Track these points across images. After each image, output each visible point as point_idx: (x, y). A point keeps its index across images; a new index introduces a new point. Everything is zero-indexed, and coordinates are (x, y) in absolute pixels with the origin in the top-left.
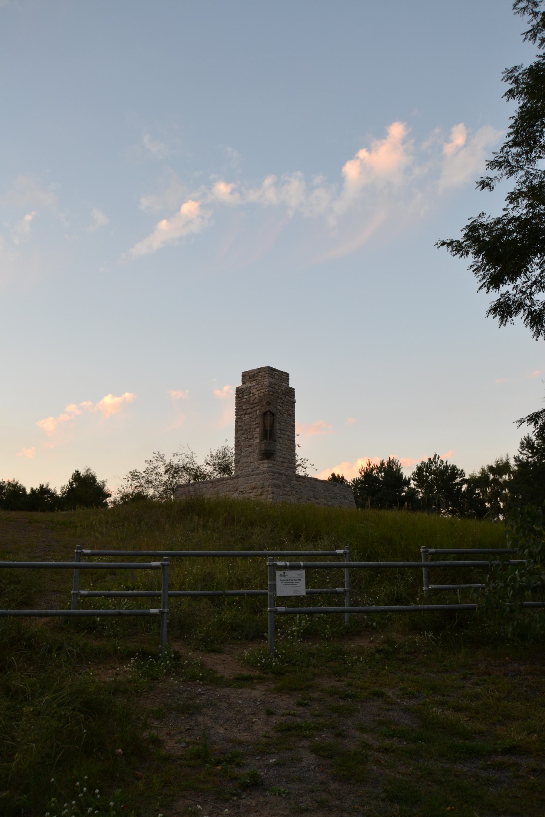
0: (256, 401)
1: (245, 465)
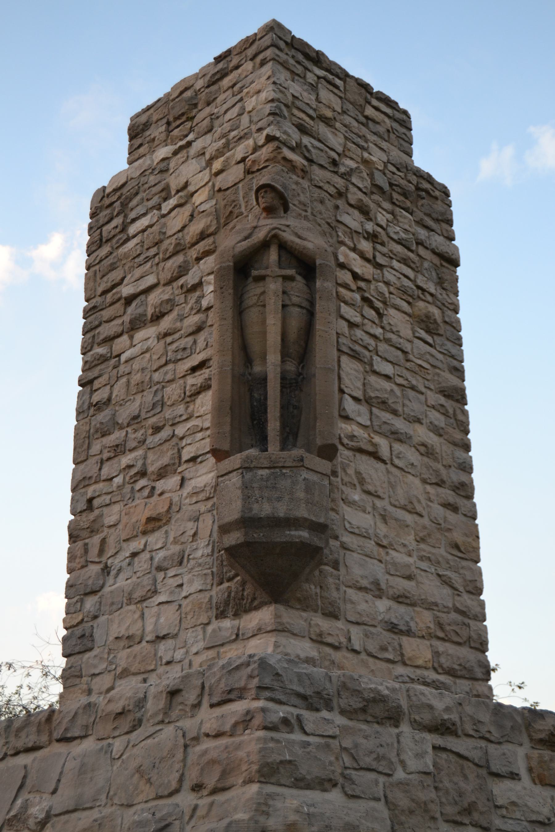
0: (195, 228)
1: (123, 658)
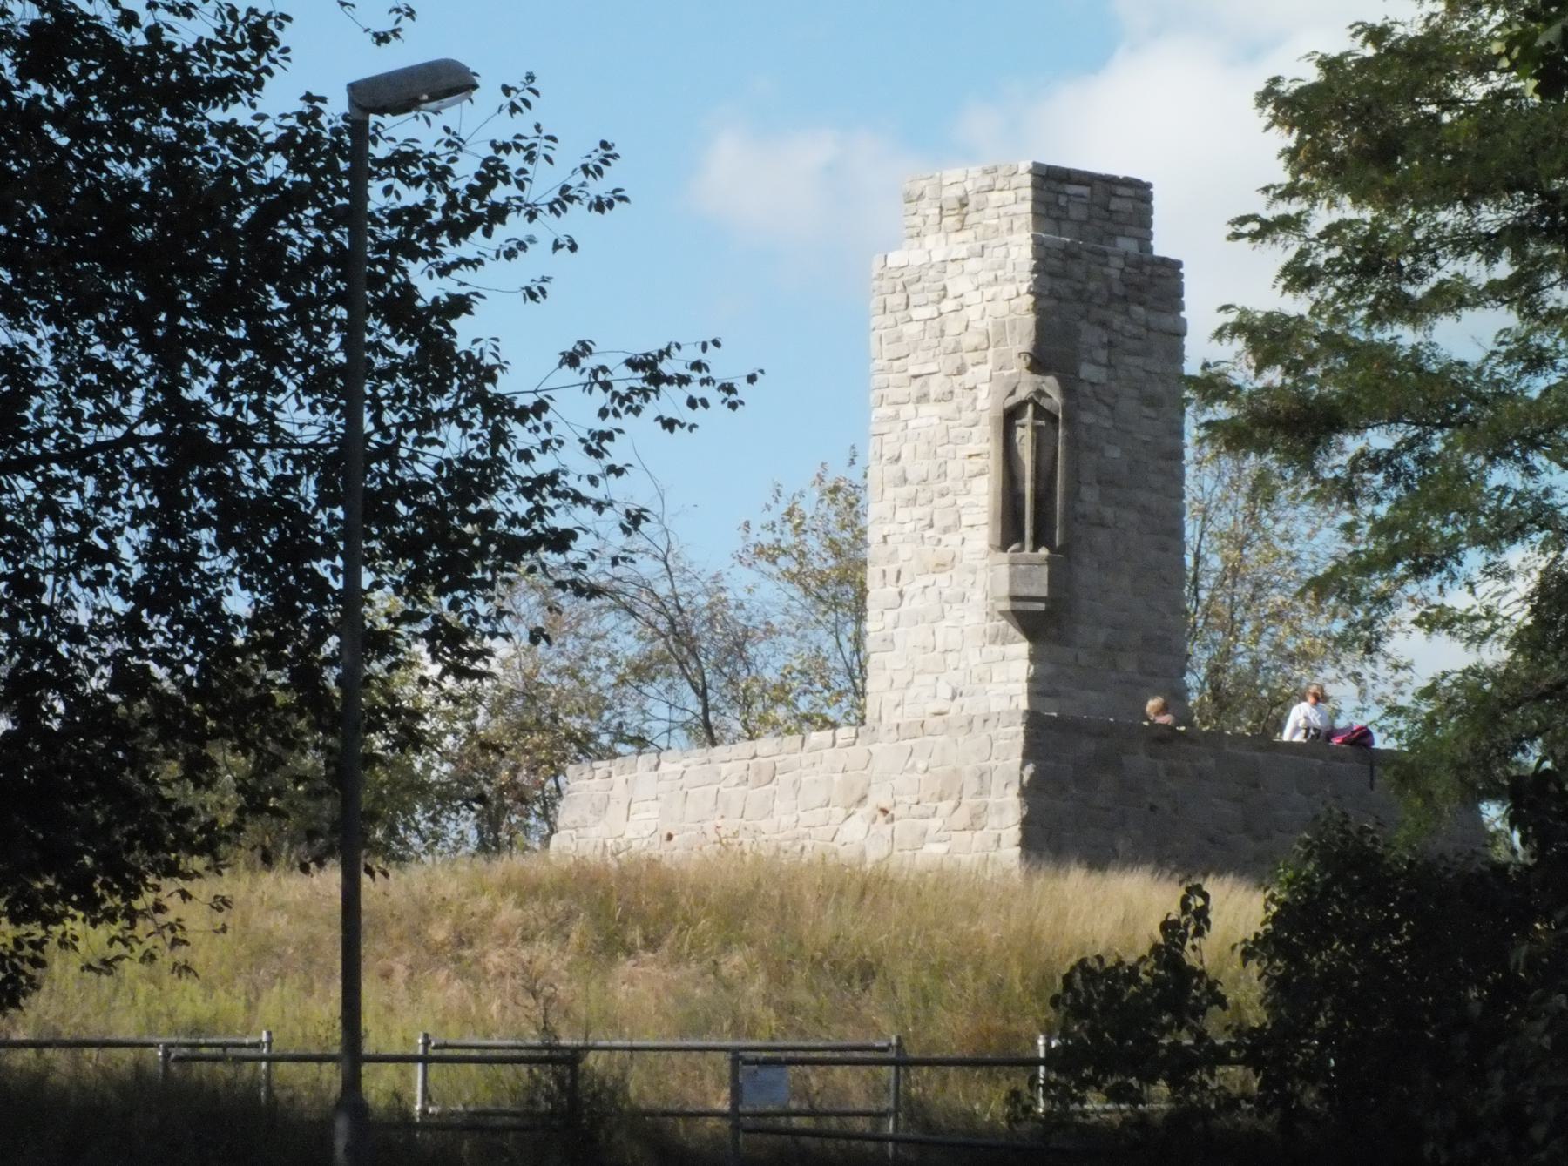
0: (970, 340)
